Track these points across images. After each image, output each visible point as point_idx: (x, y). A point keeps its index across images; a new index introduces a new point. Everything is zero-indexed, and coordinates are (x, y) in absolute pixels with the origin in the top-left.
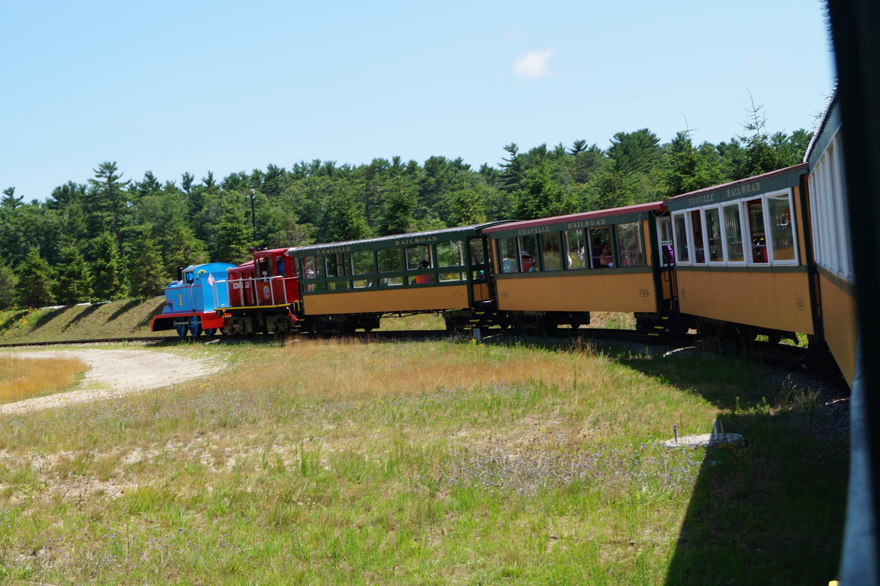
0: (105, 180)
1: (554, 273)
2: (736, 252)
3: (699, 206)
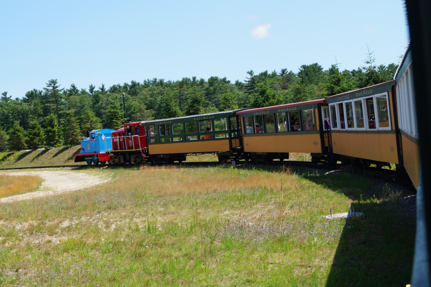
0: (51, 88)
1: (271, 134)
2: (360, 124)
3: (342, 101)
